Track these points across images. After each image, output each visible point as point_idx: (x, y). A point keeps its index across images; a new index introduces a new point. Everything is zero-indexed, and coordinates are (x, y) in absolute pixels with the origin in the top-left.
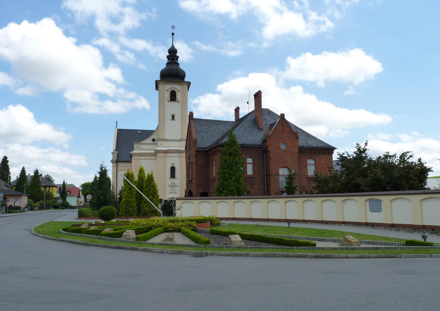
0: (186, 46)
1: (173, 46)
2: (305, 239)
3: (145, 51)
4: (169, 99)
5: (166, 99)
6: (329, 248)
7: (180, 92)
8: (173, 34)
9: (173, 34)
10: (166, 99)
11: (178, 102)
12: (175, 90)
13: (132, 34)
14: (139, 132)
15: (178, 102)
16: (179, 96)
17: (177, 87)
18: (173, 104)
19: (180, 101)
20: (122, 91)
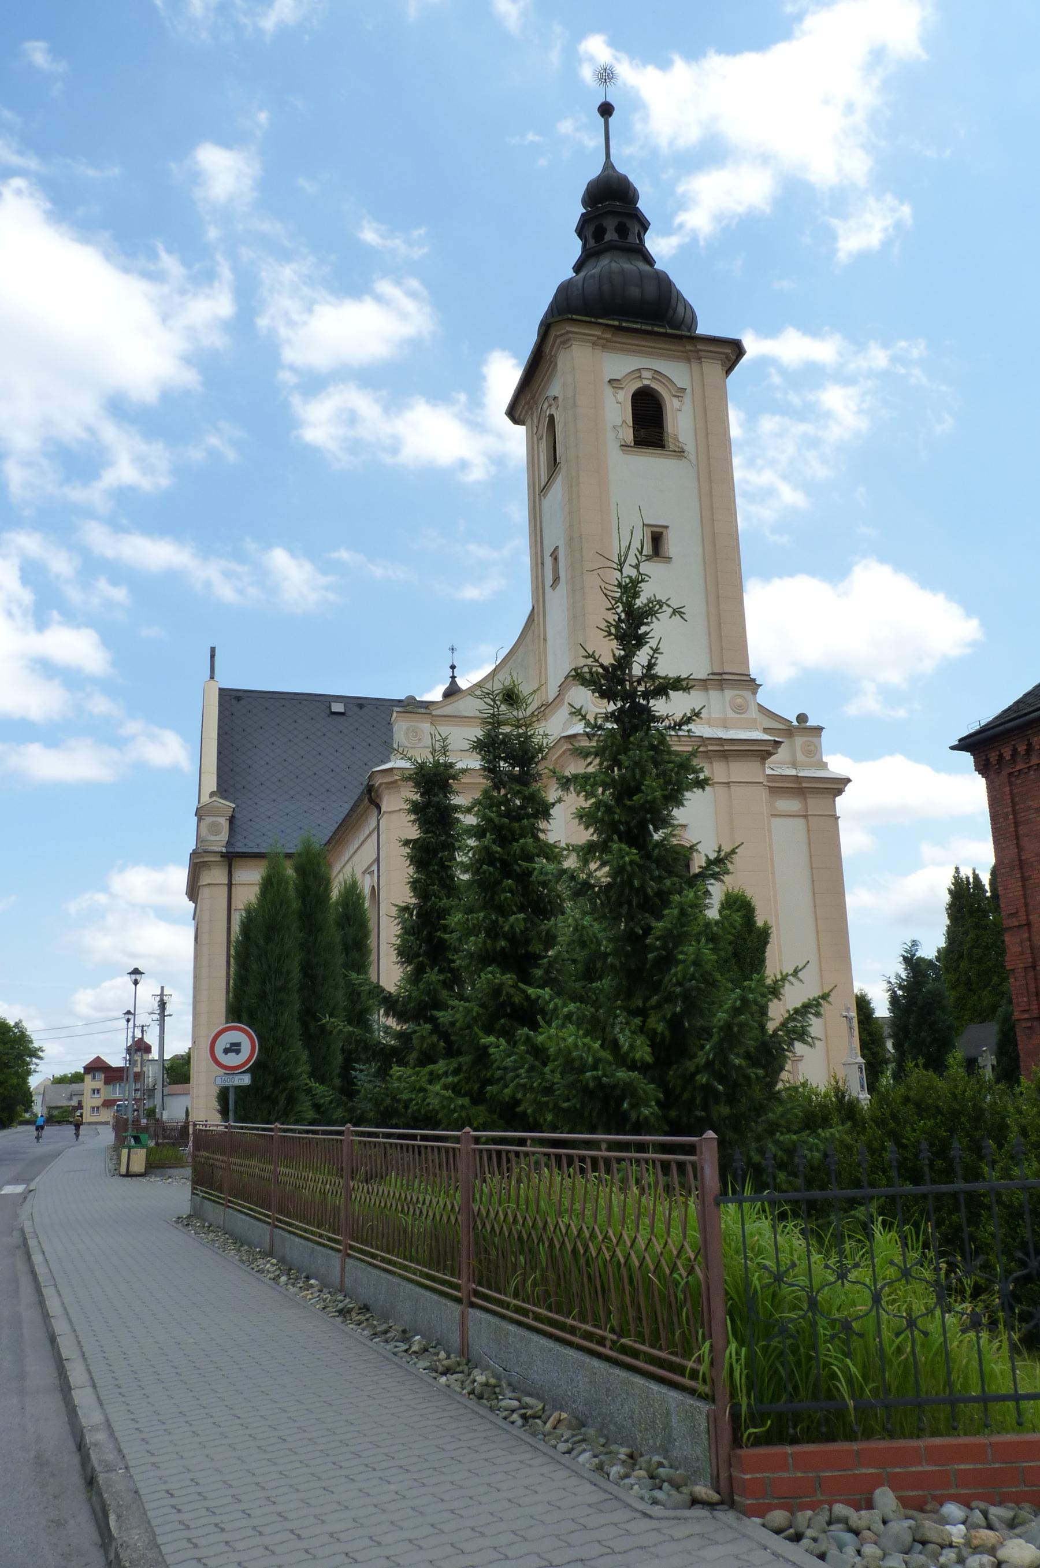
0: (308, 567)
1: (608, 165)
2: (608, 1343)
3: (172, 577)
4: (629, 435)
5: (611, 436)
6: (912, 1438)
7: (687, 399)
8: (606, 110)
9: (606, 110)
10: (611, 436)
11: (680, 453)
12: (655, 385)
13: (135, 512)
14: (337, 707)
15: (680, 453)
16: (680, 421)
17: (670, 372)
18: (648, 461)
19: (690, 447)
20: (101, 705)
